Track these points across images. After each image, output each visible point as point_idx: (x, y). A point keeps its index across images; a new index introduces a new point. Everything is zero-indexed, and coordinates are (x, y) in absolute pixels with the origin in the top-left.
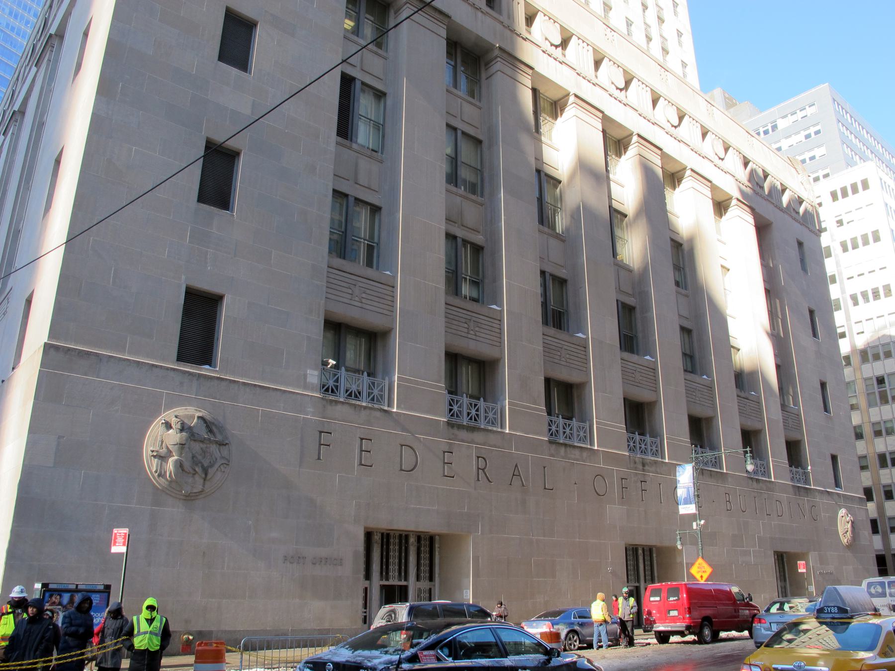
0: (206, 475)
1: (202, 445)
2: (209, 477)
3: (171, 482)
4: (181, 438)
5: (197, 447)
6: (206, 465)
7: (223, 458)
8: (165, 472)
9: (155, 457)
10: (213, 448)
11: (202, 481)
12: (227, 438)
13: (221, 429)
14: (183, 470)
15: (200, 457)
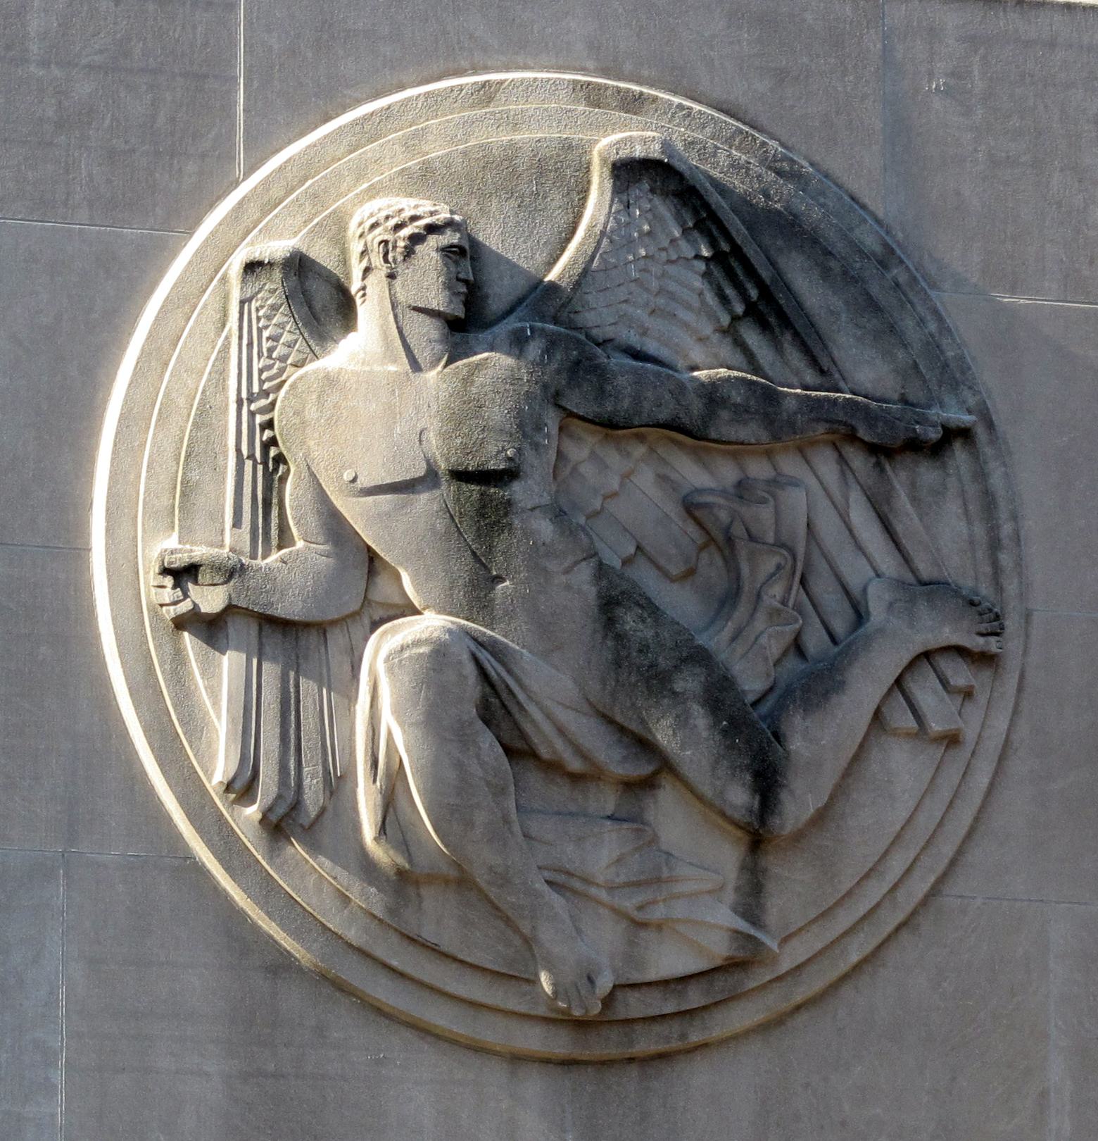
0: (767, 780)
1: (692, 473)
2: (799, 803)
3: (404, 882)
4: (463, 412)
5: (638, 491)
6: (751, 681)
7: (927, 589)
8: (337, 785)
9: (210, 628)
10: (817, 494)
11: (727, 856)
12: (954, 375)
13: (882, 279)
14: (519, 751)
15: (682, 604)
